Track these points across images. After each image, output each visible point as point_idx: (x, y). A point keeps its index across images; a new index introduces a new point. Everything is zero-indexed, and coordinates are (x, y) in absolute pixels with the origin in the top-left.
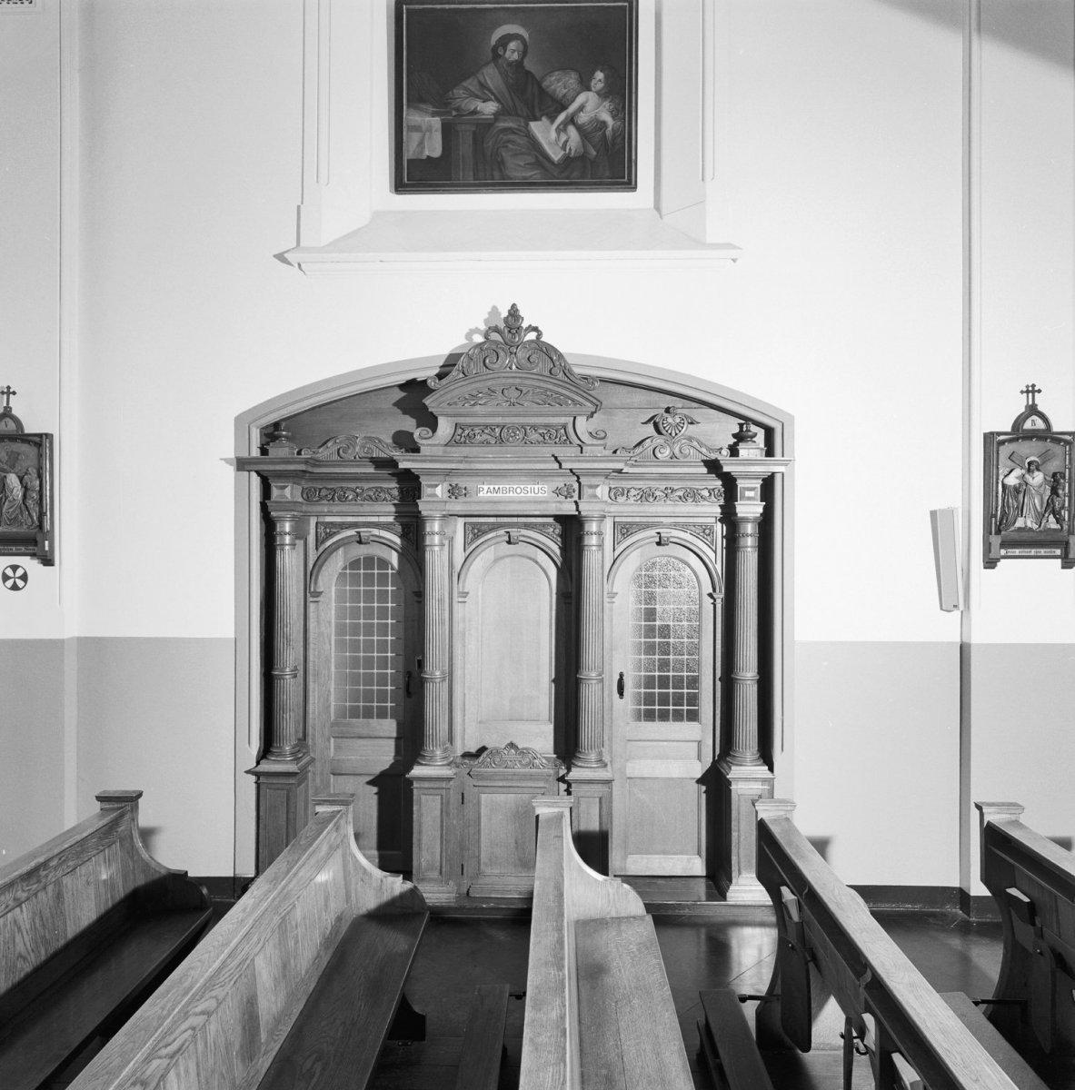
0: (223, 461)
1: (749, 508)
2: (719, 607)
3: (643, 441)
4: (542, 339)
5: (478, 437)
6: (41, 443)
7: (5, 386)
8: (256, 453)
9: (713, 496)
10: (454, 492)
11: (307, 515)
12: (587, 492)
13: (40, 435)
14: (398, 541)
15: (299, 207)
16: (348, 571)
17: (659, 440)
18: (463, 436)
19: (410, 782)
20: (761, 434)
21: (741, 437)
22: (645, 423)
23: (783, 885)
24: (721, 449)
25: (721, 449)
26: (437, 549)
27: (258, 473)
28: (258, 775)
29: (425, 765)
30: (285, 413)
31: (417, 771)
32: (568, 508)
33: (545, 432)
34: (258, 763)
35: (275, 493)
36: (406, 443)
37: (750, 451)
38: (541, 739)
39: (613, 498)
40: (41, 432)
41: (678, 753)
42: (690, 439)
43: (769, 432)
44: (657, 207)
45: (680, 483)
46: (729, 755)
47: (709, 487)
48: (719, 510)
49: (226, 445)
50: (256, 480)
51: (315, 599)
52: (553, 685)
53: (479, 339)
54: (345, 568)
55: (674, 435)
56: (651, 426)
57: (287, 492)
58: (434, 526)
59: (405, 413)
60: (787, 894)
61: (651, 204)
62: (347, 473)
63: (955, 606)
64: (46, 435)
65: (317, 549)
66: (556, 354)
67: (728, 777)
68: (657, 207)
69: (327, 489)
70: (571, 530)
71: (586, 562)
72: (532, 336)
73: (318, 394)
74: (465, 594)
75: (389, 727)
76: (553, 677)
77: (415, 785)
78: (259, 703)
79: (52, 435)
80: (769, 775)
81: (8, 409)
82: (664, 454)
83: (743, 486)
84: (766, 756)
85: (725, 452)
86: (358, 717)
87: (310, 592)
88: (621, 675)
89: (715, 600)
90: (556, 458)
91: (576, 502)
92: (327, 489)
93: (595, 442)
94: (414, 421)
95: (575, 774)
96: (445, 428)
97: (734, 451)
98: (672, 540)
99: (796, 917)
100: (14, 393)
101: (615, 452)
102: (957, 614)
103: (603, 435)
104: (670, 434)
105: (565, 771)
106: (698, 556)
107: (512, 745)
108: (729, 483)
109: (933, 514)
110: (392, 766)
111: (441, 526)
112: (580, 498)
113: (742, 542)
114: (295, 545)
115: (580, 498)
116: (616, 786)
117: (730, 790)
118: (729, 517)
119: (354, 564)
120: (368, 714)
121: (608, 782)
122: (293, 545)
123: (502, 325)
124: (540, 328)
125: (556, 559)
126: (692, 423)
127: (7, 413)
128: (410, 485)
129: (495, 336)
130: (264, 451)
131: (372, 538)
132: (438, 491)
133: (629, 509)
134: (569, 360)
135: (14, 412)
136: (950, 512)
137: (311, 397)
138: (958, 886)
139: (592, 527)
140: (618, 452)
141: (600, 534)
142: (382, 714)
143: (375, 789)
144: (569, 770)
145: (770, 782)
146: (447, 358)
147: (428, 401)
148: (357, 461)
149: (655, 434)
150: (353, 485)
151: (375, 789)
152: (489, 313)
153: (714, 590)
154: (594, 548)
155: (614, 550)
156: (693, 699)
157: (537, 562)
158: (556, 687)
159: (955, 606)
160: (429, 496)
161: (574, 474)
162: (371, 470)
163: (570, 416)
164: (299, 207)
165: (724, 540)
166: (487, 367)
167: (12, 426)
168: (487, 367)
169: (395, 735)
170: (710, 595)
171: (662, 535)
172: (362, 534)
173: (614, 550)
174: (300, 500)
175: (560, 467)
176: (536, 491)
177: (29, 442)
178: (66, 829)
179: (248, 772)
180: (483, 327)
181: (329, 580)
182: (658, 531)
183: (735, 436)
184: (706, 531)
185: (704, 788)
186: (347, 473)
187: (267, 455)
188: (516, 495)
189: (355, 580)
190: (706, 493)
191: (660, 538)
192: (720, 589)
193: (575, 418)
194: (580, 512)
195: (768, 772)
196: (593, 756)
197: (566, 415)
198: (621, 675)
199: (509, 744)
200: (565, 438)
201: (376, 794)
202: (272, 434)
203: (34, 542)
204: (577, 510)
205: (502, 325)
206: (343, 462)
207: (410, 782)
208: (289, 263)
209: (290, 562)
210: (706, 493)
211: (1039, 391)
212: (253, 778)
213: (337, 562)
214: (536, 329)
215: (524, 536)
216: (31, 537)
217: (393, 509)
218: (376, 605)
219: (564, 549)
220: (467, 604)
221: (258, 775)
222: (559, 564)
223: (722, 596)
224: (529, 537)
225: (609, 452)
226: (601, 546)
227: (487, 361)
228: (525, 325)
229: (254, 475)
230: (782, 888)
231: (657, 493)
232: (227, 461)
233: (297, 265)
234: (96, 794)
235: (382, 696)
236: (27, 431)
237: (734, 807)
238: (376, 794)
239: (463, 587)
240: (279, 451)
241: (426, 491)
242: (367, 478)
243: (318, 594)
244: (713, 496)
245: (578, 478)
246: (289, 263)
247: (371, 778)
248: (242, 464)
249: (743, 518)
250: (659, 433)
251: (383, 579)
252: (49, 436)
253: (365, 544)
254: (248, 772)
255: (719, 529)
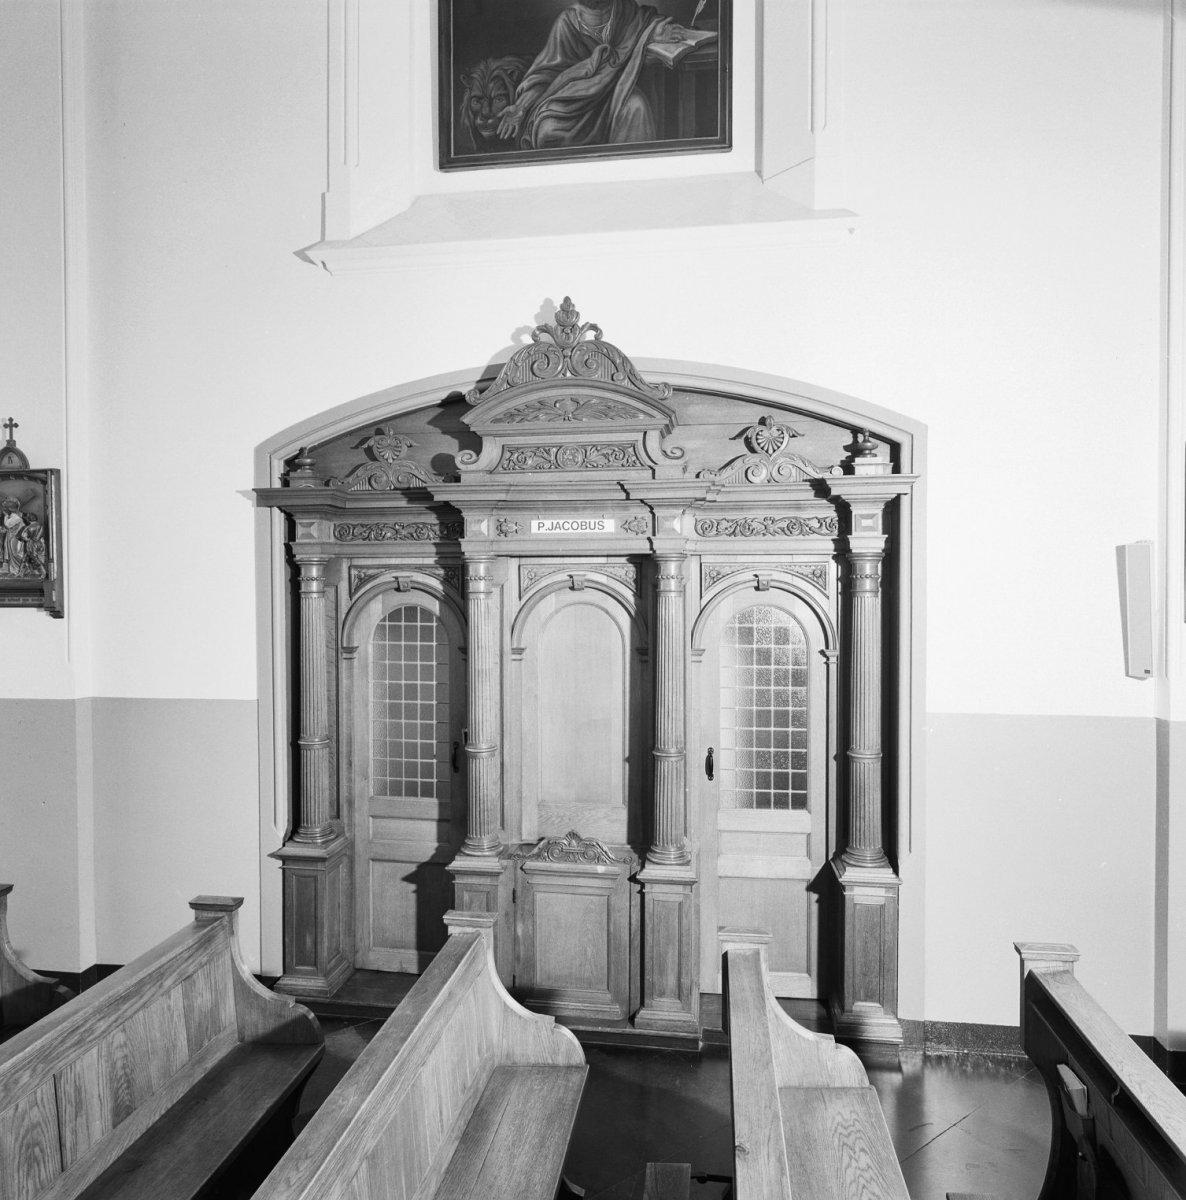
0: (239, 495)
1: (867, 540)
2: (833, 668)
3: (733, 461)
4: (603, 339)
5: (530, 462)
6: (44, 479)
7: (7, 418)
8: (277, 484)
9: (824, 527)
10: (501, 530)
11: (339, 557)
12: (660, 523)
13: (45, 471)
14: (440, 587)
15: (323, 195)
16: (387, 623)
17: (752, 459)
18: (513, 460)
19: (451, 876)
20: (884, 451)
21: (855, 450)
22: (734, 438)
23: (1061, 1063)
24: (832, 467)
25: (832, 467)
26: (482, 596)
27: (280, 508)
28: (285, 859)
29: (468, 855)
30: (309, 442)
31: (458, 863)
32: (642, 547)
33: (610, 452)
34: (284, 845)
35: (300, 531)
36: (446, 469)
37: (874, 465)
38: (611, 826)
39: (701, 532)
40: (46, 467)
41: (782, 848)
42: (791, 456)
43: (895, 449)
44: (759, 172)
45: (782, 512)
46: (845, 852)
47: (819, 517)
48: (832, 546)
49: (247, 477)
50: (279, 517)
51: (348, 656)
52: (627, 765)
53: (528, 340)
54: (384, 620)
55: (771, 451)
56: (741, 441)
57: (314, 531)
58: (478, 569)
59: (444, 433)
60: (1072, 1081)
61: (752, 168)
62: (379, 502)
63: (1147, 672)
64: (51, 470)
65: (520, 598)
66: (620, 356)
67: (840, 880)
68: (759, 172)
69: (362, 526)
70: (646, 567)
71: (662, 612)
72: (590, 335)
73: (371, 409)
74: (519, 651)
75: (431, 806)
76: (627, 755)
77: (458, 881)
78: (286, 775)
79: (58, 471)
80: (896, 881)
81: (11, 443)
82: (760, 477)
83: (860, 512)
84: (890, 854)
85: (838, 472)
86: (400, 795)
87: (342, 650)
88: (710, 751)
89: (828, 659)
90: (622, 486)
91: (649, 539)
92: (362, 526)
93: (668, 461)
94: (456, 442)
95: (650, 872)
96: (491, 451)
97: (848, 468)
98: (773, 584)
99: (1080, 1106)
100: (11, 420)
101: (698, 476)
102: (1151, 681)
103: (679, 453)
104: (767, 452)
105: (639, 868)
106: (810, 606)
107: (573, 835)
108: (843, 509)
109: (1121, 551)
110: (433, 857)
111: (487, 569)
112: (654, 534)
113: (472, 586)
114: (324, 592)
115: (654, 534)
116: (704, 887)
117: (843, 897)
118: (843, 554)
119: (394, 615)
120: (412, 791)
121: (690, 884)
122: (322, 593)
123: (553, 323)
124: (599, 326)
125: (630, 609)
126: (794, 436)
127: (11, 448)
128: (452, 522)
129: (545, 337)
130: (286, 483)
131: (586, 584)
132: (484, 527)
133: (719, 551)
134: (638, 367)
135: (18, 446)
136: (1143, 547)
137: (361, 413)
138: (1152, 1035)
139: (671, 568)
140: (701, 475)
141: (680, 578)
142: (427, 792)
143: (413, 887)
144: (643, 867)
145: (894, 888)
146: (485, 371)
147: (466, 419)
148: (384, 495)
149: (745, 451)
150: (391, 521)
151: (413, 887)
152: (542, 307)
153: (827, 647)
154: (315, 595)
155: (701, 597)
156: (801, 782)
157: (607, 612)
158: (630, 766)
159: (1147, 672)
160: (871, 516)
161: (646, 504)
162: (403, 503)
163: (638, 431)
164: (323, 195)
165: (840, 584)
166: (533, 374)
167: (16, 462)
168: (533, 374)
169: (436, 816)
170: (822, 653)
171: (761, 578)
172: (400, 580)
173: (701, 597)
174: (332, 540)
175: (628, 498)
176: (592, 527)
177: (35, 479)
178: (737, 1159)
179: (272, 855)
180: (534, 325)
181: (366, 636)
182: (395, 574)
183: (846, 448)
184: (817, 578)
185: (815, 897)
186: (379, 502)
187: (288, 486)
188: (588, 530)
189: (395, 633)
190: (815, 524)
191: (573, 583)
192: (835, 648)
193: (645, 433)
194: (654, 552)
195: (894, 876)
196: (673, 852)
197: (633, 431)
198: (710, 751)
199: (570, 834)
200: (634, 458)
201: (414, 892)
202: (292, 464)
203: (41, 592)
204: (652, 549)
205: (553, 323)
206: (373, 494)
207: (451, 876)
208: (312, 262)
209: (315, 608)
210: (815, 524)
211: (16, 425)
212: (280, 863)
213: (376, 610)
214: (594, 327)
215: (589, 581)
216: (37, 589)
217: (433, 549)
218: (403, 662)
219: (639, 594)
220: (523, 662)
221: (285, 859)
222: (633, 613)
223: (837, 653)
224: (597, 583)
225: (690, 475)
226: (683, 591)
227: (535, 365)
228: (580, 324)
229: (276, 511)
230: (1058, 1066)
231: (754, 525)
232: (244, 493)
233: (321, 265)
234: (189, 900)
235: (427, 771)
236: (33, 466)
237: (848, 919)
238: (414, 892)
239: (519, 642)
240: (303, 481)
241: (471, 528)
242: (396, 511)
243: (351, 650)
244: (824, 527)
245: (651, 508)
246: (312, 262)
247: (413, 868)
248: (264, 497)
249: (860, 555)
250: (753, 450)
251: (426, 634)
252: (56, 472)
253: (579, 590)
254: (272, 855)
255: (833, 570)
